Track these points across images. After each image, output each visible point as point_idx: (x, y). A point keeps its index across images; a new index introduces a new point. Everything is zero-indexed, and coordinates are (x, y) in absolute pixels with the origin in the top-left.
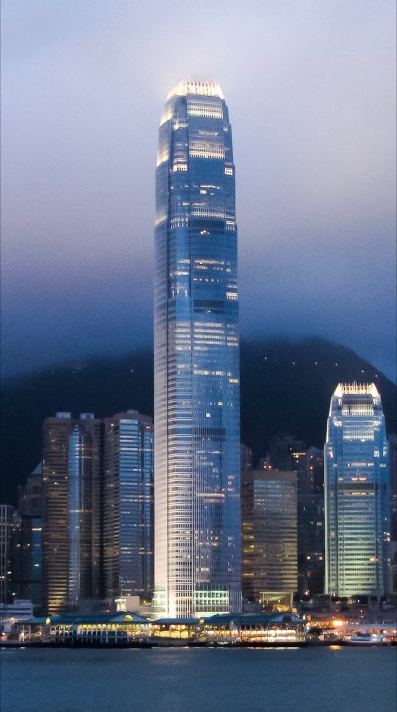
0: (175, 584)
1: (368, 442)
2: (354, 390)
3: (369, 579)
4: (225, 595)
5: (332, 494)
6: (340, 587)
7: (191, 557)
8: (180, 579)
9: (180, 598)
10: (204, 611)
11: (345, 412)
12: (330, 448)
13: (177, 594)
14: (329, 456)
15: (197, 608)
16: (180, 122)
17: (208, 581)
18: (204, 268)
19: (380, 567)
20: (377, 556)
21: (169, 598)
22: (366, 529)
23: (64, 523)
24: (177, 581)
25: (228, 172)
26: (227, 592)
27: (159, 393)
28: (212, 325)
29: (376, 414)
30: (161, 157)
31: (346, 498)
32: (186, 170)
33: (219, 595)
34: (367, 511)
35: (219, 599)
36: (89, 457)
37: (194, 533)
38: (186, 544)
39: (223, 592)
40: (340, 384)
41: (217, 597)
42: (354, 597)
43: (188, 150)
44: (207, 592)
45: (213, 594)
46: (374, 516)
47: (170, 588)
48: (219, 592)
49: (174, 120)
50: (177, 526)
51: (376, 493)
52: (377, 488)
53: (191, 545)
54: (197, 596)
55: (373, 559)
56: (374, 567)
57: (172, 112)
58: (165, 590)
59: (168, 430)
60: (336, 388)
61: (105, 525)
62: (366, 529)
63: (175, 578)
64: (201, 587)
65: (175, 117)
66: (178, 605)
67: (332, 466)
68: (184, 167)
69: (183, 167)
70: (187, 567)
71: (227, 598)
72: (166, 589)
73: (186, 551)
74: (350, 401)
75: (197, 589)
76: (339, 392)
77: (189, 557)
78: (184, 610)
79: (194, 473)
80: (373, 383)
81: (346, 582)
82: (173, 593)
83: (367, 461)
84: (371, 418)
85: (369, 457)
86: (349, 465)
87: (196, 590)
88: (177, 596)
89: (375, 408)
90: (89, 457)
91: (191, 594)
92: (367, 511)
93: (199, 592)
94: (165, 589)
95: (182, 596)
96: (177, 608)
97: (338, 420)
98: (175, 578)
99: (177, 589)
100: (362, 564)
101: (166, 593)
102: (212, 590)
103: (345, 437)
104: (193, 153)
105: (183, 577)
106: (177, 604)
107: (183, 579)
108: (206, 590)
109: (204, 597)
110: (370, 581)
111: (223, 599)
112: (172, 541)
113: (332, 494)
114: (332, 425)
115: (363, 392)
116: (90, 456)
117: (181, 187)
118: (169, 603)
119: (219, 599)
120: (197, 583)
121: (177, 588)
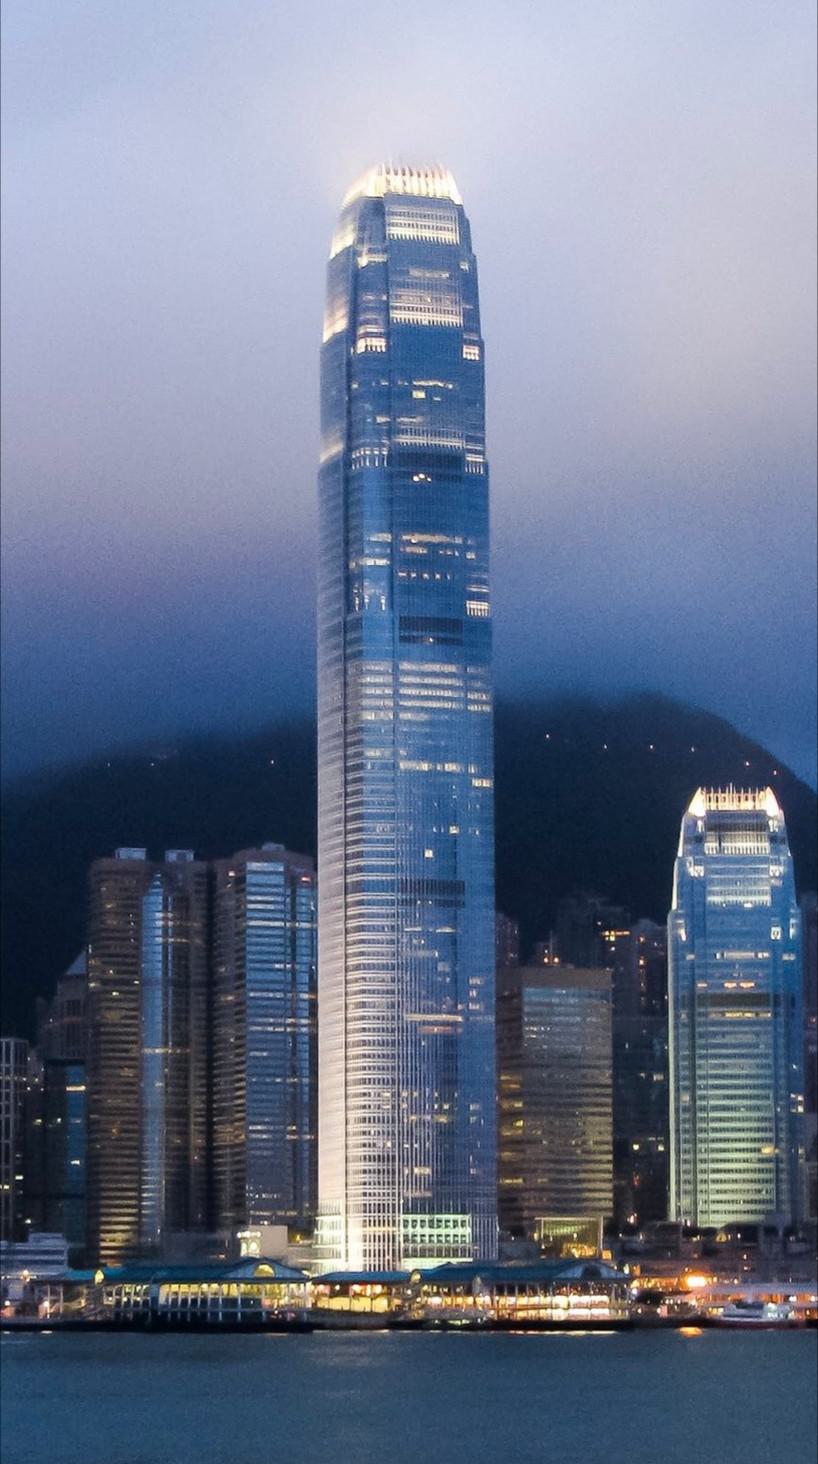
0: (361, 1200)
1: (759, 909)
2: (730, 802)
3: (760, 1191)
4: (463, 1224)
5: (683, 1016)
6: (701, 1207)
7: (393, 1146)
8: (372, 1191)
9: (371, 1230)
10: (421, 1256)
11: (711, 846)
12: (681, 921)
13: (365, 1221)
14: (677, 938)
15: (406, 1250)
16: (370, 251)
17: (428, 1194)
18: (421, 551)
19: (782, 1166)
20: (777, 1143)
21: (349, 1229)
22: (754, 1087)
23: (131, 1075)
24: (365, 1194)
25: (470, 353)
26: (467, 1218)
27: (327, 808)
28: (436, 668)
29: (774, 850)
30: (332, 324)
31: (714, 1024)
32: (384, 350)
33: (451, 1224)
34: (756, 1051)
35: (451, 1232)
36: (184, 940)
37: (399, 1096)
38: (384, 1118)
39: (459, 1217)
40: (700, 790)
41: (446, 1227)
42: (730, 1228)
43: (386, 308)
44: (427, 1217)
45: (439, 1221)
46: (770, 1061)
47: (351, 1209)
48: (452, 1217)
49: (359, 248)
50: (364, 1082)
51: (775, 1015)
52: (776, 1004)
53: (393, 1121)
54: (405, 1226)
55: (768, 1150)
56: (771, 1166)
57: (354, 230)
58: (339, 1214)
59: (346, 883)
60: (692, 797)
61: (215, 1080)
62: (754, 1087)
63: (361, 1189)
64: (414, 1207)
65: (360, 240)
66: (367, 1243)
67: (684, 958)
68: (380, 344)
69: (378, 344)
70: (385, 1166)
71: (468, 1231)
72: (343, 1210)
73: (383, 1132)
74: (721, 824)
75: (406, 1212)
76: (699, 805)
77: (389, 1144)
78: (379, 1253)
79: (400, 972)
80: (768, 788)
81: (713, 1197)
82: (356, 1220)
83: (757, 948)
84: (765, 860)
85: (759, 939)
86: (718, 956)
87: (404, 1213)
88: (365, 1226)
89: (773, 839)
90: (184, 940)
91: (394, 1222)
92: (756, 1051)
93: (410, 1217)
94: (341, 1211)
95: (375, 1225)
96: (365, 1250)
97: (697, 863)
98: (361, 1189)
99: (365, 1212)
100: (746, 1161)
101: (341, 1219)
102: (438, 1213)
103: (712, 899)
104: (397, 315)
105: (377, 1186)
106: (365, 1241)
107: (376, 1191)
108: (425, 1213)
109: (421, 1228)
110: (763, 1196)
111: (460, 1231)
112: (354, 1112)
113: (683, 1016)
114: (683, 874)
115: (747, 806)
116: (186, 938)
117: (374, 384)
118: (349, 1240)
119: (451, 1232)
120: (406, 1200)
121: (366, 1208)
